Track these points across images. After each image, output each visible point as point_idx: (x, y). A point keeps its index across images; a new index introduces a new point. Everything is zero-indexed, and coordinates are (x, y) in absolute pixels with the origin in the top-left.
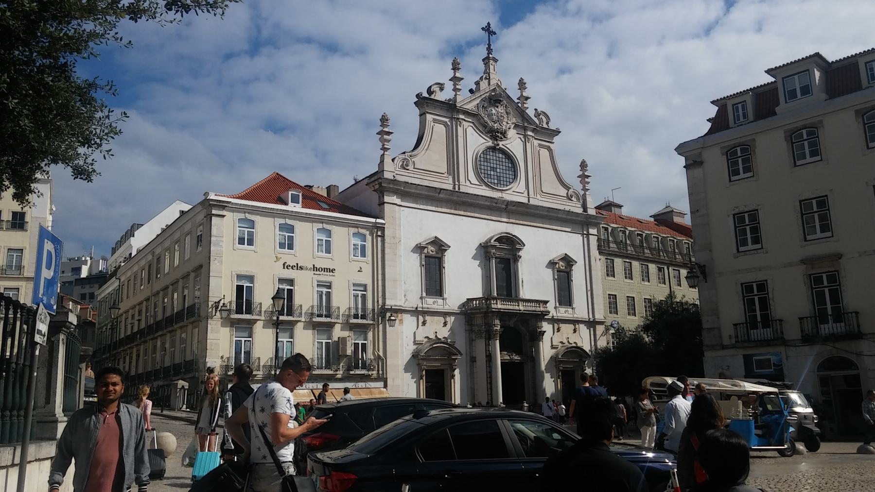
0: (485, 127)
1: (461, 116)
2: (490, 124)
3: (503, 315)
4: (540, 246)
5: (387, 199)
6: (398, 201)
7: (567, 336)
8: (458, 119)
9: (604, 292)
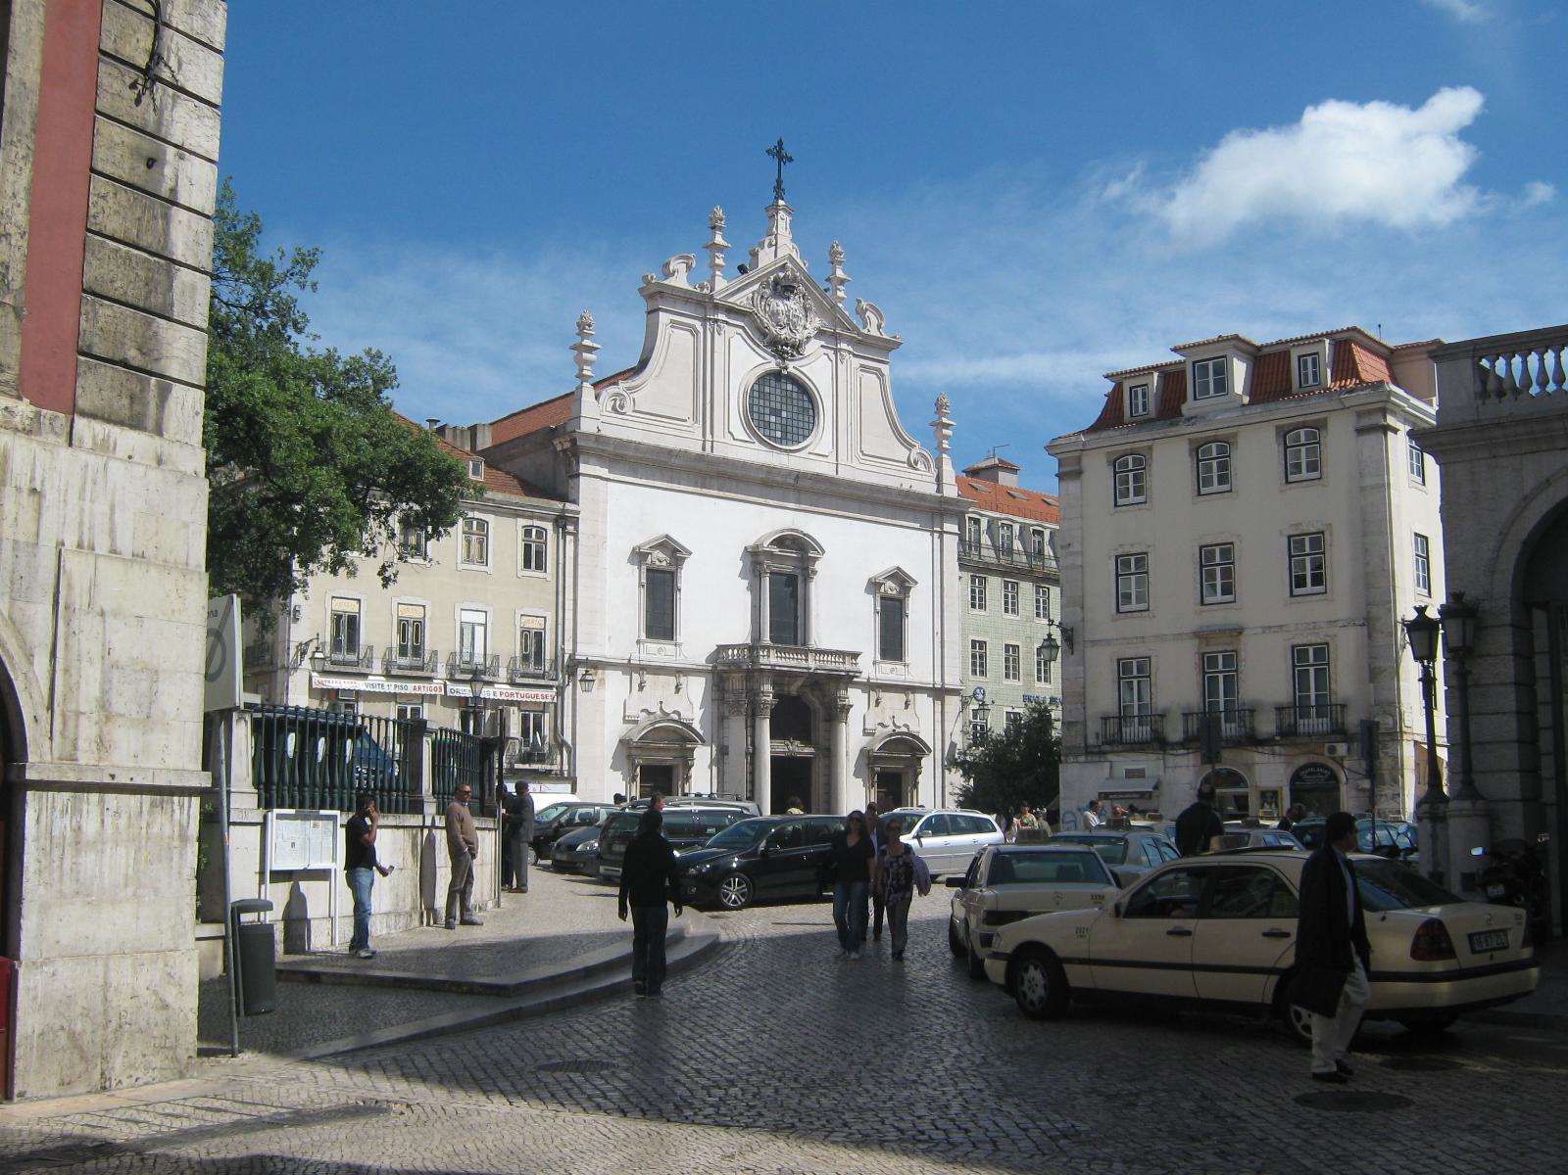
0: (765, 335)
1: (722, 317)
2: (774, 330)
3: (779, 677)
4: (851, 555)
5: (583, 468)
6: (604, 472)
7: (895, 715)
8: (716, 321)
9: (964, 635)
